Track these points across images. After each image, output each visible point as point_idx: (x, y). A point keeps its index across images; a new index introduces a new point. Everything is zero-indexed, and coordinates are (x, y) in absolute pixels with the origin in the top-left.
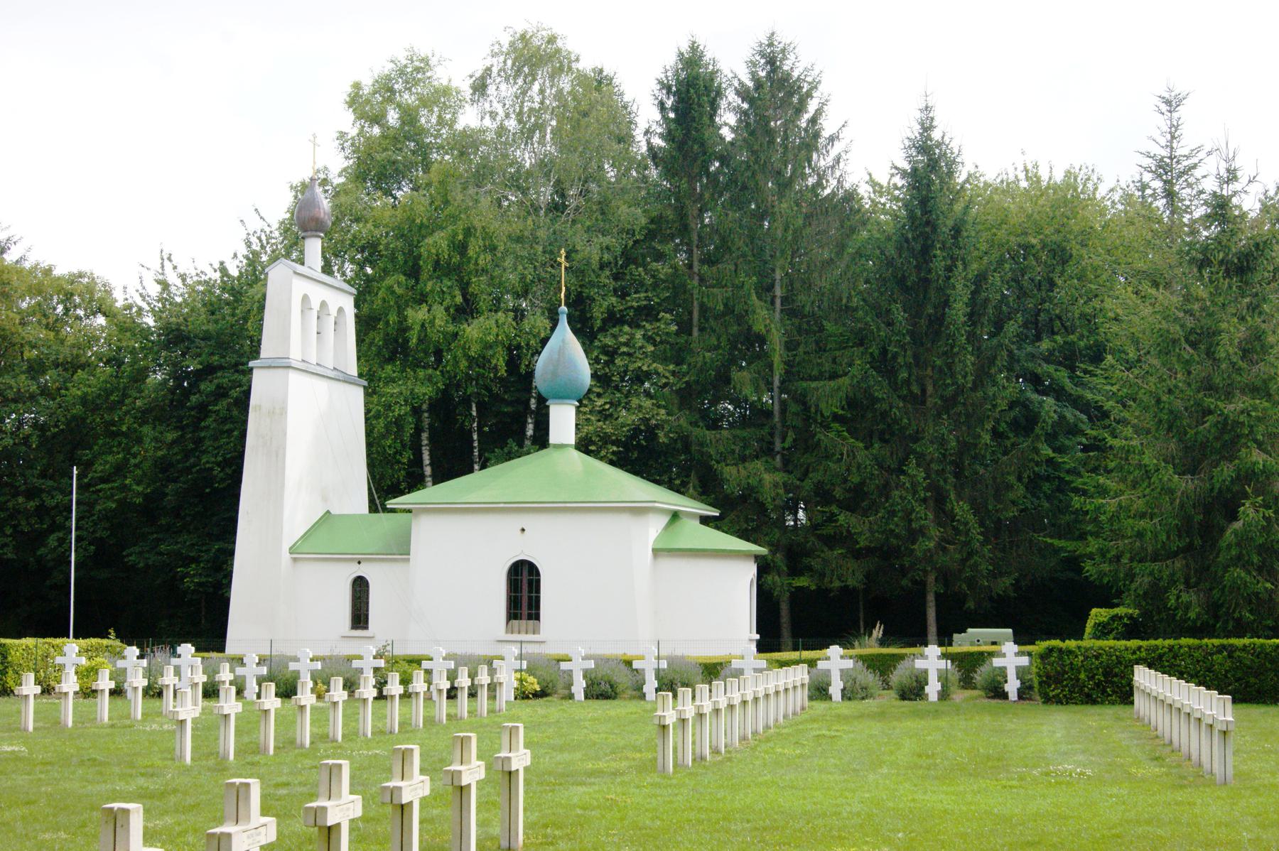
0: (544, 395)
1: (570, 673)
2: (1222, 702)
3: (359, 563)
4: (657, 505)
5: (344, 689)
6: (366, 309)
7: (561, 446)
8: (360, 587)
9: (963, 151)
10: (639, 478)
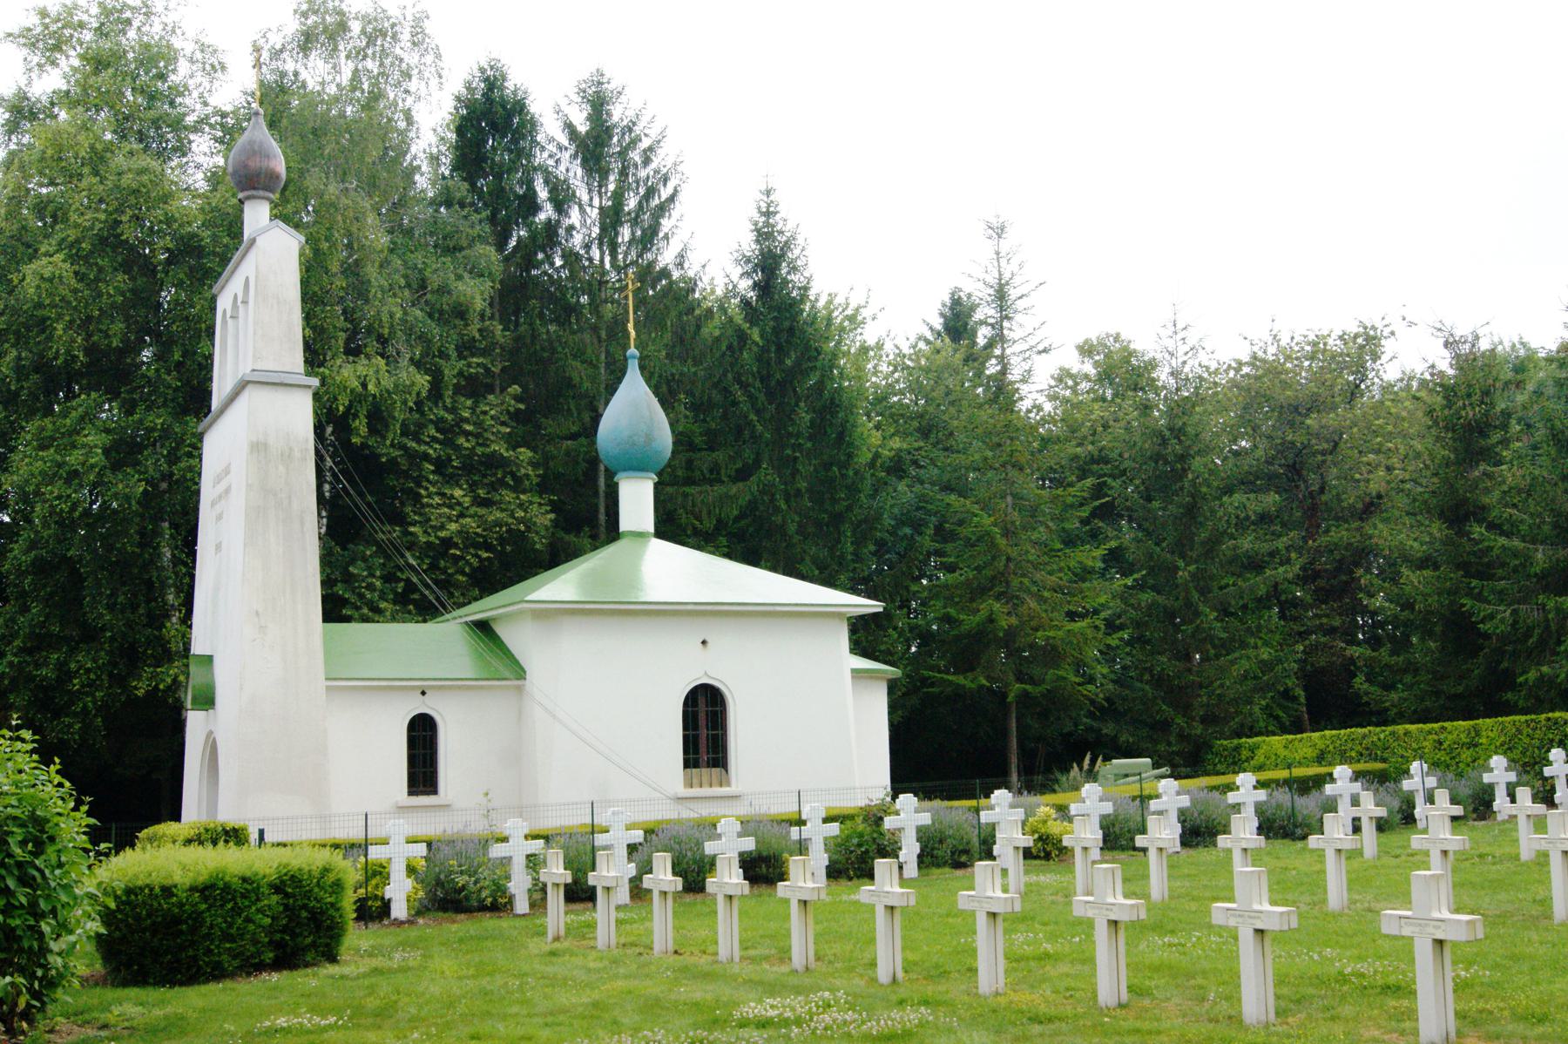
0: (613, 469)
1: (506, 861)
2: (801, 864)
3: (423, 693)
4: (587, 606)
5: (594, 888)
6: (654, 382)
7: (640, 535)
8: (422, 734)
9: (681, 197)
10: (198, 548)
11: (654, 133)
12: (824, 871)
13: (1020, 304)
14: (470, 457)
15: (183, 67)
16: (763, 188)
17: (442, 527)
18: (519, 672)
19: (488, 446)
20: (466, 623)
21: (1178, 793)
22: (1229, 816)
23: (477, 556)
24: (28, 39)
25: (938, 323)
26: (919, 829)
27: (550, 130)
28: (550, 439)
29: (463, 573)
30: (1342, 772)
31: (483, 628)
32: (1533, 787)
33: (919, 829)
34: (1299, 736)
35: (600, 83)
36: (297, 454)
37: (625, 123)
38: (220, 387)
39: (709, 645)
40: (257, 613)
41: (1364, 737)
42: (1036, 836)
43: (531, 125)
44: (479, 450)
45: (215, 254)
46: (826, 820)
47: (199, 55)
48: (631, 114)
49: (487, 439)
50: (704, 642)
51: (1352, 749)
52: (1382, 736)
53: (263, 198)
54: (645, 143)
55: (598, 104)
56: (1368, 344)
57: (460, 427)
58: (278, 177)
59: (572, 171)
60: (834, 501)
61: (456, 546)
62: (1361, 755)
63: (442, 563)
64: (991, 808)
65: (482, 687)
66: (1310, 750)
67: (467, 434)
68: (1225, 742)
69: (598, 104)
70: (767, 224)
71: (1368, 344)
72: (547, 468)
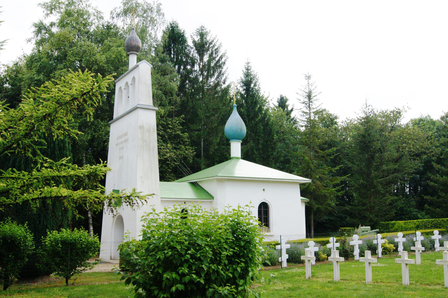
7: (238, 158)
11: (218, 44)
12: (286, 260)
13: (315, 98)
14: (171, 135)
15: (92, 18)
16: (247, 62)
17: (165, 155)
18: (211, 197)
19: (176, 132)
20: (190, 183)
21: (359, 240)
22: (443, 241)
23: (174, 163)
24: (45, 6)
25: (277, 104)
26: (359, 245)
27: (190, 43)
28: (192, 130)
29: (170, 169)
30: (436, 232)
31: (194, 184)
32: (425, 240)
33: (359, 245)
34: (409, 221)
35: (202, 30)
36: (152, 130)
37: (210, 41)
38: (118, 111)
39: (265, 190)
40: (141, 178)
41: (432, 221)
42: (383, 248)
43: (185, 41)
44: (173, 133)
45: (108, 71)
46: (286, 243)
47: (96, 14)
48: (212, 39)
49: (176, 130)
50: (264, 190)
51: (428, 225)
52: (439, 221)
53: (135, 54)
54: (216, 47)
55: (202, 35)
56: (397, 114)
57: (168, 126)
58: (140, 48)
59: (194, 53)
60: (268, 151)
61: (168, 161)
62: (432, 226)
63: (164, 166)
64: (353, 240)
65: (204, 202)
66: (414, 225)
67: (170, 128)
68: (384, 222)
69: (202, 35)
70: (248, 73)
71: (397, 114)
72: (191, 139)
